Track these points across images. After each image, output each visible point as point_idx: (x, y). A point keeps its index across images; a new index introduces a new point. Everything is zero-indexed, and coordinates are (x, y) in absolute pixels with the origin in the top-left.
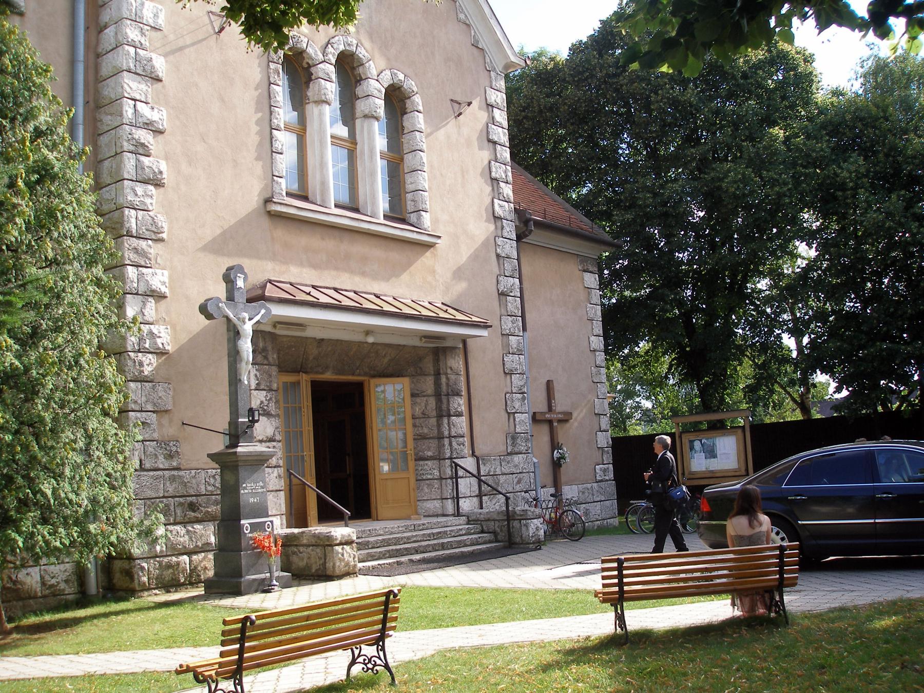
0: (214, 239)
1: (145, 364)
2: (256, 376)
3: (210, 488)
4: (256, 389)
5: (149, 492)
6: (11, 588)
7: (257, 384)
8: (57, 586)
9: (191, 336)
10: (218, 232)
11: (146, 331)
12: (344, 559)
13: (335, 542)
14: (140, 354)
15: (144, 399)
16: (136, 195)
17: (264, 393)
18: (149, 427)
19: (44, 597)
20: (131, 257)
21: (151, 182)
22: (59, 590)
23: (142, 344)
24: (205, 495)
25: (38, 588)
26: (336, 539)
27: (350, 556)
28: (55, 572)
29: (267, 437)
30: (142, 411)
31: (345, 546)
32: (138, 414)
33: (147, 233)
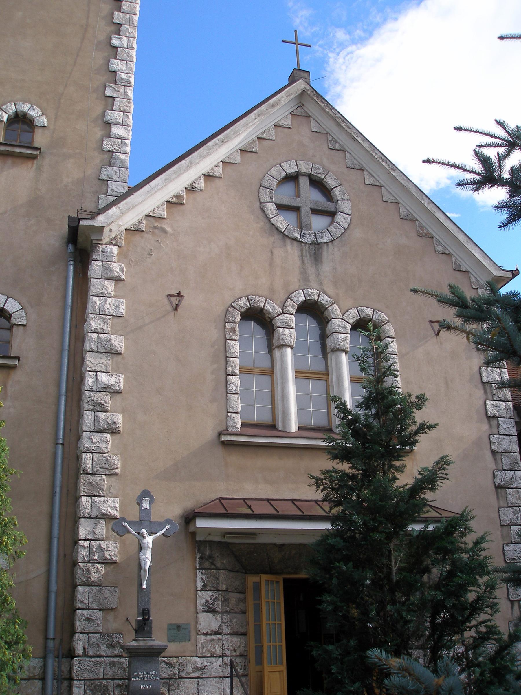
1: (92, 572)
2: (202, 579)
5: (89, 674)
7: (203, 586)
15: (91, 600)
16: (92, 442)
17: (210, 593)
20: (86, 490)
21: (107, 431)
23: (91, 556)
29: (212, 631)
30: (88, 609)
32: (85, 612)
33: (101, 470)
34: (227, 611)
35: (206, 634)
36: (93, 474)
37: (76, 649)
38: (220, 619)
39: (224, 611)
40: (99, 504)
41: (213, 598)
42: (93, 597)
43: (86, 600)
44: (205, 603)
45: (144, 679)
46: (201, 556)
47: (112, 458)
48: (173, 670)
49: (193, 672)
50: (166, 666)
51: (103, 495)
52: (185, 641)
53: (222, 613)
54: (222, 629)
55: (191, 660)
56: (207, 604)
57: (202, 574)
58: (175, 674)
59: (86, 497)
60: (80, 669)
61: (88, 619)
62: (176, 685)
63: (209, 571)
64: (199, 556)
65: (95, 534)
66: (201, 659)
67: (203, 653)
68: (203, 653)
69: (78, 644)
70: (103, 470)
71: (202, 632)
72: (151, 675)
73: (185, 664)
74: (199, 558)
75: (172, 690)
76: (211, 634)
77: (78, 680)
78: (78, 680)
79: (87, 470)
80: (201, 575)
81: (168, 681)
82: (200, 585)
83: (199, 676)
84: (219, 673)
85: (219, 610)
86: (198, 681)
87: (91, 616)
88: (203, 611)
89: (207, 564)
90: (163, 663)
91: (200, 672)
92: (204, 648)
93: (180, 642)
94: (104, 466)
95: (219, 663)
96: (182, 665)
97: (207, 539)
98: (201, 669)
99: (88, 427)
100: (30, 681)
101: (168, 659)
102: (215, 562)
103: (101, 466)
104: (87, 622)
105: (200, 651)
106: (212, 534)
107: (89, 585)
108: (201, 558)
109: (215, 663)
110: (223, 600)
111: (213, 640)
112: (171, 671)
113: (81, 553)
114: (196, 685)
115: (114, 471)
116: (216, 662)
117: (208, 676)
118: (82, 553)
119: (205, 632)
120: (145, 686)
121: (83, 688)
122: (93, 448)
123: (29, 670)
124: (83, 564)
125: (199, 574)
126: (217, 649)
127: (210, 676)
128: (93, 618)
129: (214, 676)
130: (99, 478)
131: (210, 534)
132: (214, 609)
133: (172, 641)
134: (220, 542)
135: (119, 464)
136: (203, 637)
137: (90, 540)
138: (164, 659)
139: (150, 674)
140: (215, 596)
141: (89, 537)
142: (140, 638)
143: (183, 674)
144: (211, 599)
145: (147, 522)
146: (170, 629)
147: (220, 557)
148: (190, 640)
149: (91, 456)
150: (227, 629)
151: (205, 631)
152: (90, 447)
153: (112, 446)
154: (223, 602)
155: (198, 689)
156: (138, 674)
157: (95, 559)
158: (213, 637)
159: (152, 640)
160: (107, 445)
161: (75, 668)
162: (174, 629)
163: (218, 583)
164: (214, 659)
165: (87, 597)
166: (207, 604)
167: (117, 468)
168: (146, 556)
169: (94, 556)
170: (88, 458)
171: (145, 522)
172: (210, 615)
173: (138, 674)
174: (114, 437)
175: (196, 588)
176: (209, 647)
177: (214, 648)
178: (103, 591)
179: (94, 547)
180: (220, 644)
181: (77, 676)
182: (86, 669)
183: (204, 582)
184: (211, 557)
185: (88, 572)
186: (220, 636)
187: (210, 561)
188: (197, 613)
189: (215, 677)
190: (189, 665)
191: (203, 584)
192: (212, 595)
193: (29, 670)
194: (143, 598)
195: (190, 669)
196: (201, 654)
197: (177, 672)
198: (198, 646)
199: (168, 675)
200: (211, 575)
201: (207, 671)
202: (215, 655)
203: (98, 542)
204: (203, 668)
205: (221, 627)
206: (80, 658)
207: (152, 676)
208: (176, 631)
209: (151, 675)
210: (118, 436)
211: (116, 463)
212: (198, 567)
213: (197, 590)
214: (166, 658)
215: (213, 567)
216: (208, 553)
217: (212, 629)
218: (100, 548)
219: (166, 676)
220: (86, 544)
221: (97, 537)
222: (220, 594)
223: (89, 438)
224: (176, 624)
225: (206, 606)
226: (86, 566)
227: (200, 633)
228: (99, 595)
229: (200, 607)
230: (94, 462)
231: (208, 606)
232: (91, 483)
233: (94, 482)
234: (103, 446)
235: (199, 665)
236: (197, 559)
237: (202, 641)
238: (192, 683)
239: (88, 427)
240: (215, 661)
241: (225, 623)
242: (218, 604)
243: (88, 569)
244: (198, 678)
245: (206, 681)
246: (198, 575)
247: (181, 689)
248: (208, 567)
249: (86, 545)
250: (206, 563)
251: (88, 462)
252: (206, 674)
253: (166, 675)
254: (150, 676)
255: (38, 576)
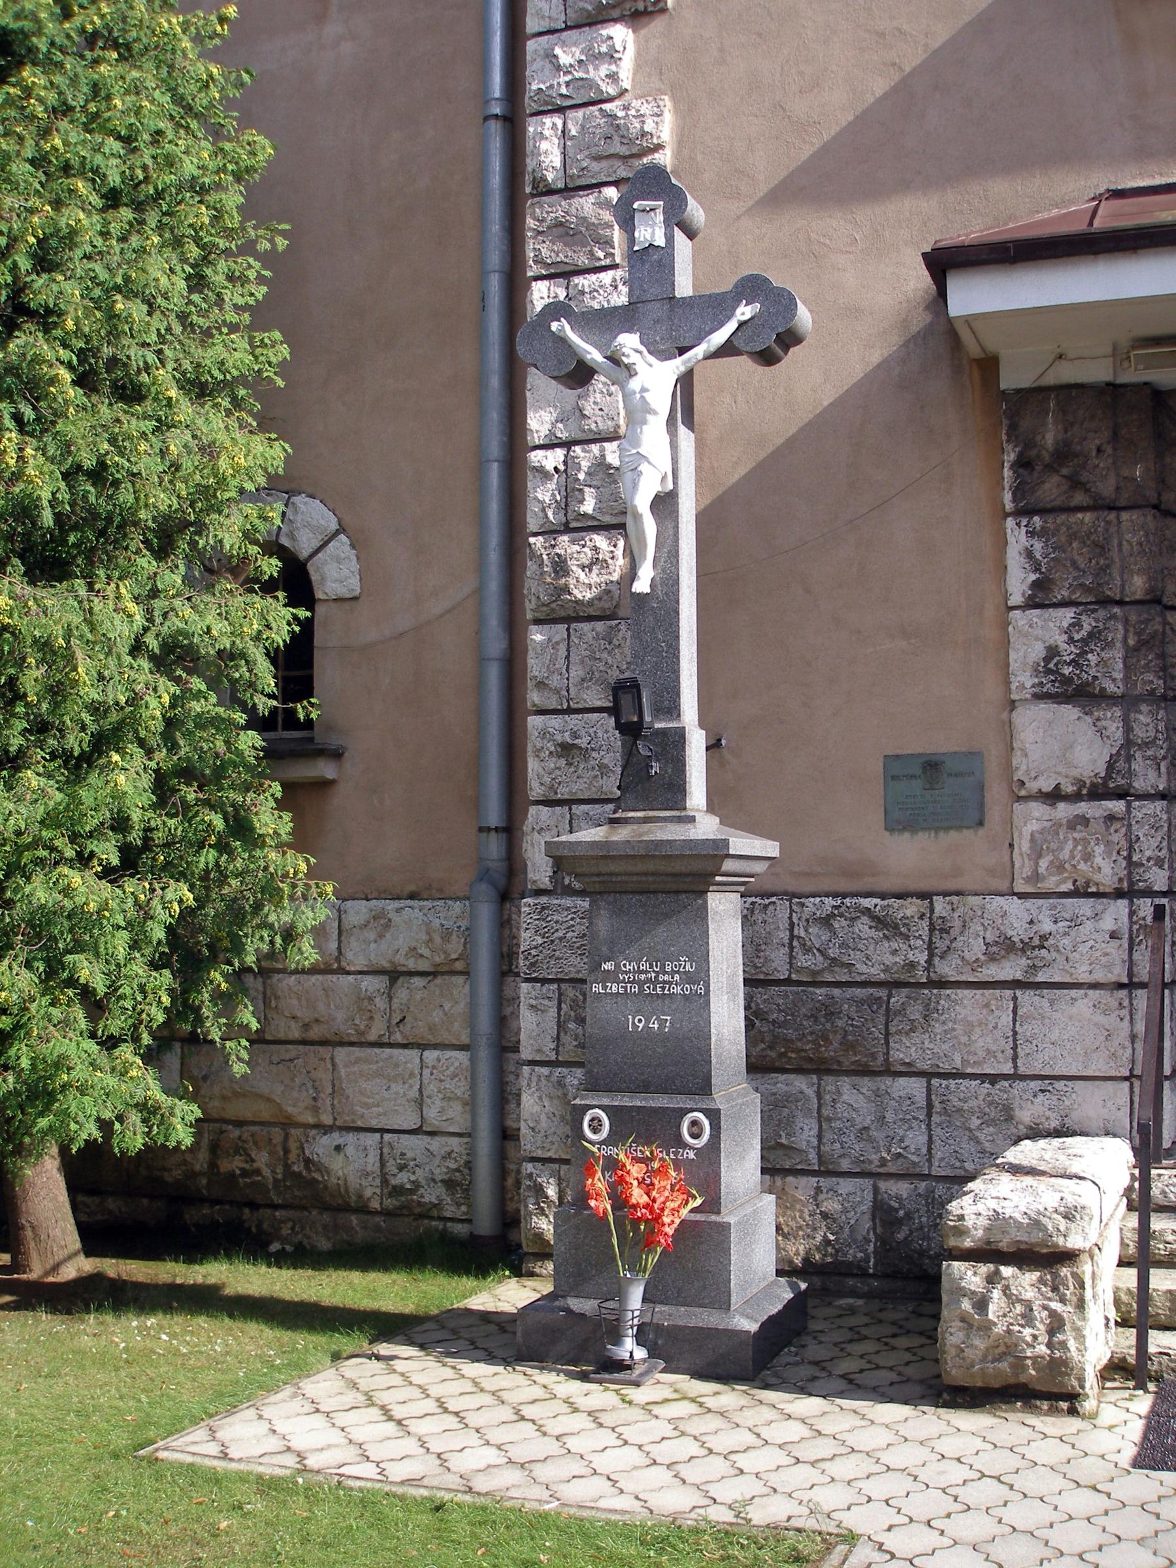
0: (862, 121)
1: (573, 566)
2: (1029, 554)
3: (803, 960)
4: (1031, 603)
5: (575, 960)
6: (300, 1173)
7: (1036, 585)
8: (412, 1192)
9: (763, 454)
10: (879, 86)
11: (585, 465)
12: (987, 1326)
13: (952, 1242)
14: (564, 539)
15: (576, 672)
16: (558, 68)
17: (1066, 616)
18: (586, 760)
19: (386, 1213)
20: (545, 252)
21: (616, 13)
22: (419, 1204)
23: (572, 503)
24: (788, 982)
25: (371, 1191)
26: (961, 1232)
27: (1028, 1318)
28: (410, 1155)
29: (1080, 783)
30: (570, 711)
31: (1007, 1271)
32: (554, 722)
33: (595, 166)
34: (1152, 692)
35: (1054, 796)
36: (570, 190)
37: (530, 868)
38: (1115, 729)
39: (1139, 690)
40: (594, 298)
41: (1077, 637)
42: (582, 662)
43: (556, 677)
44: (1047, 660)
45: (641, 990)
46: (1020, 456)
47: (633, 112)
48: (905, 947)
49: (992, 958)
50: (873, 933)
51: (608, 262)
52: (959, 828)
53: (1128, 702)
54: (1130, 773)
55: (983, 907)
56: (1051, 666)
57: (1031, 534)
58: (912, 965)
59: (546, 283)
60: (540, 940)
61: (566, 750)
62: (915, 1012)
63: (1062, 518)
64: (1012, 456)
65: (584, 416)
66: (1029, 903)
67: (1036, 877)
68: (1036, 877)
69: (532, 844)
70: (604, 164)
71: (1033, 786)
72: (673, 972)
73: (957, 923)
74: (1011, 467)
75: (899, 1032)
76: (1076, 797)
77: (535, 980)
78: (535, 980)
79: (544, 179)
80: (1023, 537)
81: (882, 993)
82: (1019, 582)
83: (1019, 975)
84: (1108, 967)
85: (1111, 688)
86: (1015, 999)
87: (575, 735)
88: (1038, 697)
89: (1051, 489)
90: (865, 919)
91: (1024, 962)
92: (1040, 856)
93: (937, 830)
94: (603, 148)
95: (1108, 924)
96: (942, 931)
97: (1050, 380)
98: (1026, 947)
99: (543, 17)
100: (439, 980)
101: (886, 902)
102: (1085, 476)
103: (594, 150)
104: (563, 762)
105: (1023, 868)
106: (1071, 355)
107: (568, 620)
108: (1023, 464)
109: (1089, 925)
110: (1131, 642)
111: (1084, 821)
112: (895, 952)
113: (536, 498)
114: (1007, 1018)
115: (645, 160)
116: (1096, 916)
117: (1057, 979)
118: (540, 497)
119: (1047, 785)
120: (648, 1021)
121: (553, 1012)
122: (564, 91)
123: (431, 940)
124: (541, 538)
125: (1017, 537)
126: (1098, 860)
127: (1067, 979)
128: (583, 742)
129: (1084, 978)
130: (592, 199)
131: (1060, 357)
132: (1088, 684)
133: (904, 829)
134: (1113, 388)
135: (665, 130)
136: (1038, 810)
137: (567, 445)
138: (867, 903)
139: (668, 969)
140: (1088, 624)
141: (563, 434)
142: (631, 814)
143: (947, 969)
144: (1071, 640)
145: (658, 305)
146: (893, 778)
147: (1109, 450)
148: (981, 823)
149: (559, 123)
150: (1152, 774)
151: (1046, 784)
152: (551, 86)
153: (638, 67)
154: (1130, 653)
155: (1015, 1033)
156: (617, 966)
157: (585, 515)
158: (1083, 808)
159: (680, 820)
160: (613, 68)
161: (523, 934)
162: (913, 777)
163: (1104, 570)
164: (1085, 906)
165: (561, 663)
166: (1051, 666)
167: (659, 147)
168: (642, 451)
169: (582, 501)
170: (547, 133)
171: (650, 306)
172: (1070, 712)
173: (617, 966)
174: (643, 32)
175: (1006, 599)
176: (1065, 854)
177: (1088, 857)
178: (621, 634)
179: (579, 469)
180: (1118, 837)
181: (532, 964)
182: (561, 939)
183: (1037, 570)
184: (1062, 454)
185: (561, 566)
186: (1118, 806)
187: (1065, 471)
188: (1012, 705)
189: (1095, 986)
190: (976, 927)
191: (1033, 577)
192: (1077, 624)
193: (431, 940)
194: (647, 638)
195: (977, 949)
196: (1028, 880)
197: (922, 958)
198: (1016, 850)
199: (884, 971)
200: (1073, 536)
201: (1054, 955)
202: (1093, 889)
203: (595, 448)
204: (1036, 942)
205: (1121, 764)
206: (544, 900)
207: (677, 977)
208: (917, 785)
209: (673, 972)
210: (658, 24)
211: (649, 127)
212: (1009, 506)
213: (1010, 604)
214: (878, 901)
215: (1079, 498)
216: (1050, 437)
217: (1075, 773)
218: (601, 465)
219: (875, 972)
220: (552, 459)
221: (593, 426)
222: (1113, 617)
223: (547, 56)
224: (920, 755)
225: (1048, 671)
226: (553, 546)
227: (1023, 793)
228: (605, 655)
229: (1024, 680)
230: (569, 143)
231: (1056, 672)
232: (561, 224)
233: (574, 219)
234: (598, 73)
235: (1018, 930)
236: (1007, 473)
237: (1033, 826)
238: (987, 1005)
239: (543, 17)
240: (1089, 913)
241: (1147, 745)
242: (1102, 662)
243: (559, 555)
244: (1016, 984)
245: (1052, 1003)
246: (1011, 539)
247: (938, 1028)
248: (1058, 503)
249: (549, 466)
250: (1047, 486)
251: (544, 146)
252: (1049, 971)
253: (873, 971)
254: (666, 978)
255: (453, 608)
